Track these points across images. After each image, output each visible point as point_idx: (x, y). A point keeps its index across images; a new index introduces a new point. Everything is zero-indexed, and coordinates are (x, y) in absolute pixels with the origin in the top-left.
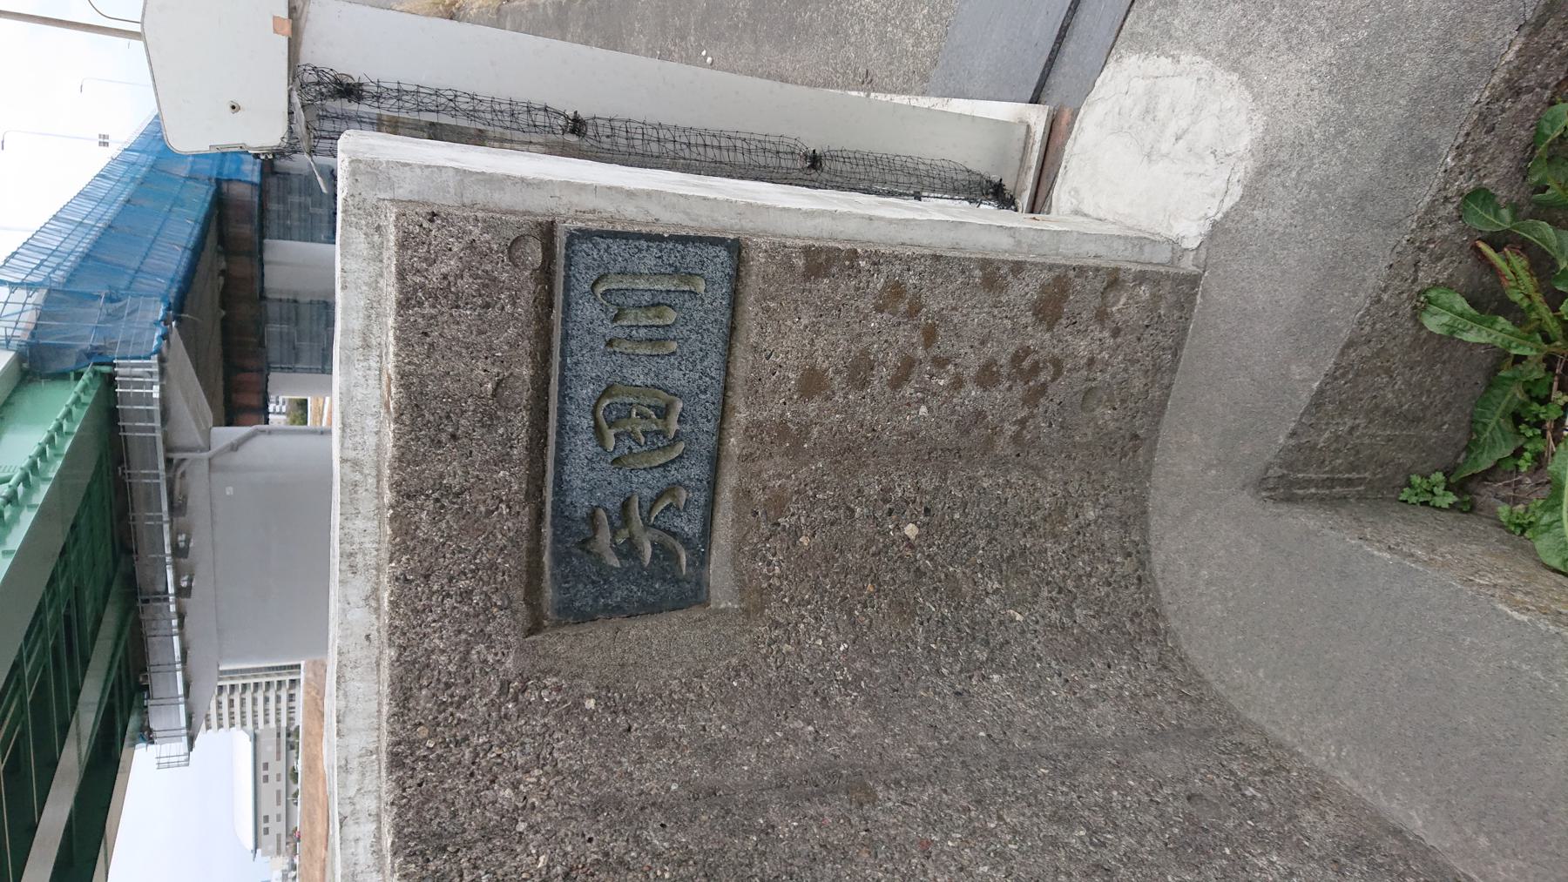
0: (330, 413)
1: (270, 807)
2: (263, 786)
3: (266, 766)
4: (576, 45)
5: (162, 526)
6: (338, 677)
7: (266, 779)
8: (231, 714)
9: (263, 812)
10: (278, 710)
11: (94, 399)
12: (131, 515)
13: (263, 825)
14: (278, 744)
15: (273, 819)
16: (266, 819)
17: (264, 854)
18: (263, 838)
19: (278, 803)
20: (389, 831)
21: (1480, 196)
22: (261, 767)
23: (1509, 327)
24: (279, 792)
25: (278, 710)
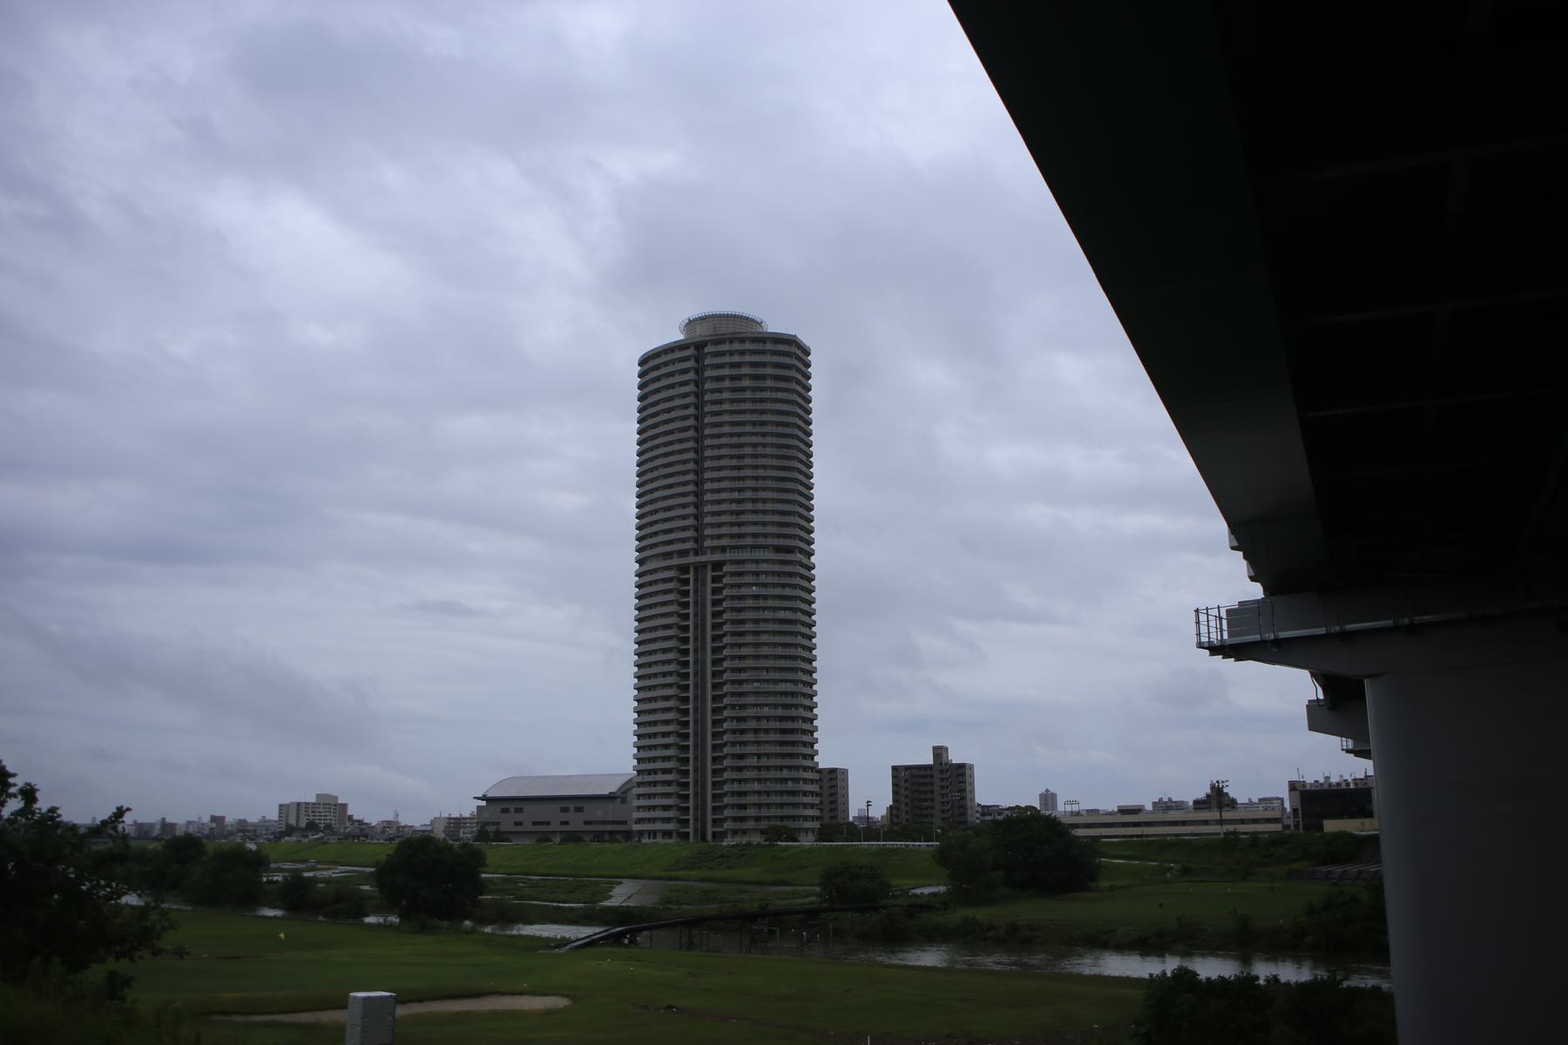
0: (702, 880)
1: (531, 814)
2: (557, 806)
5: (1228, 628)
6: (1177, 809)
8: (655, 771)
9: (527, 807)
10: (654, 820)
11: (1310, 791)
13: (512, 807)
14: (603, 823)
15: (519, 817)
16: (519, 810)
17: (479, 807)
18: (498, 807)
19: (535, 823)
20: (890, 958)
24: (548, 823)
25: (654, 820)
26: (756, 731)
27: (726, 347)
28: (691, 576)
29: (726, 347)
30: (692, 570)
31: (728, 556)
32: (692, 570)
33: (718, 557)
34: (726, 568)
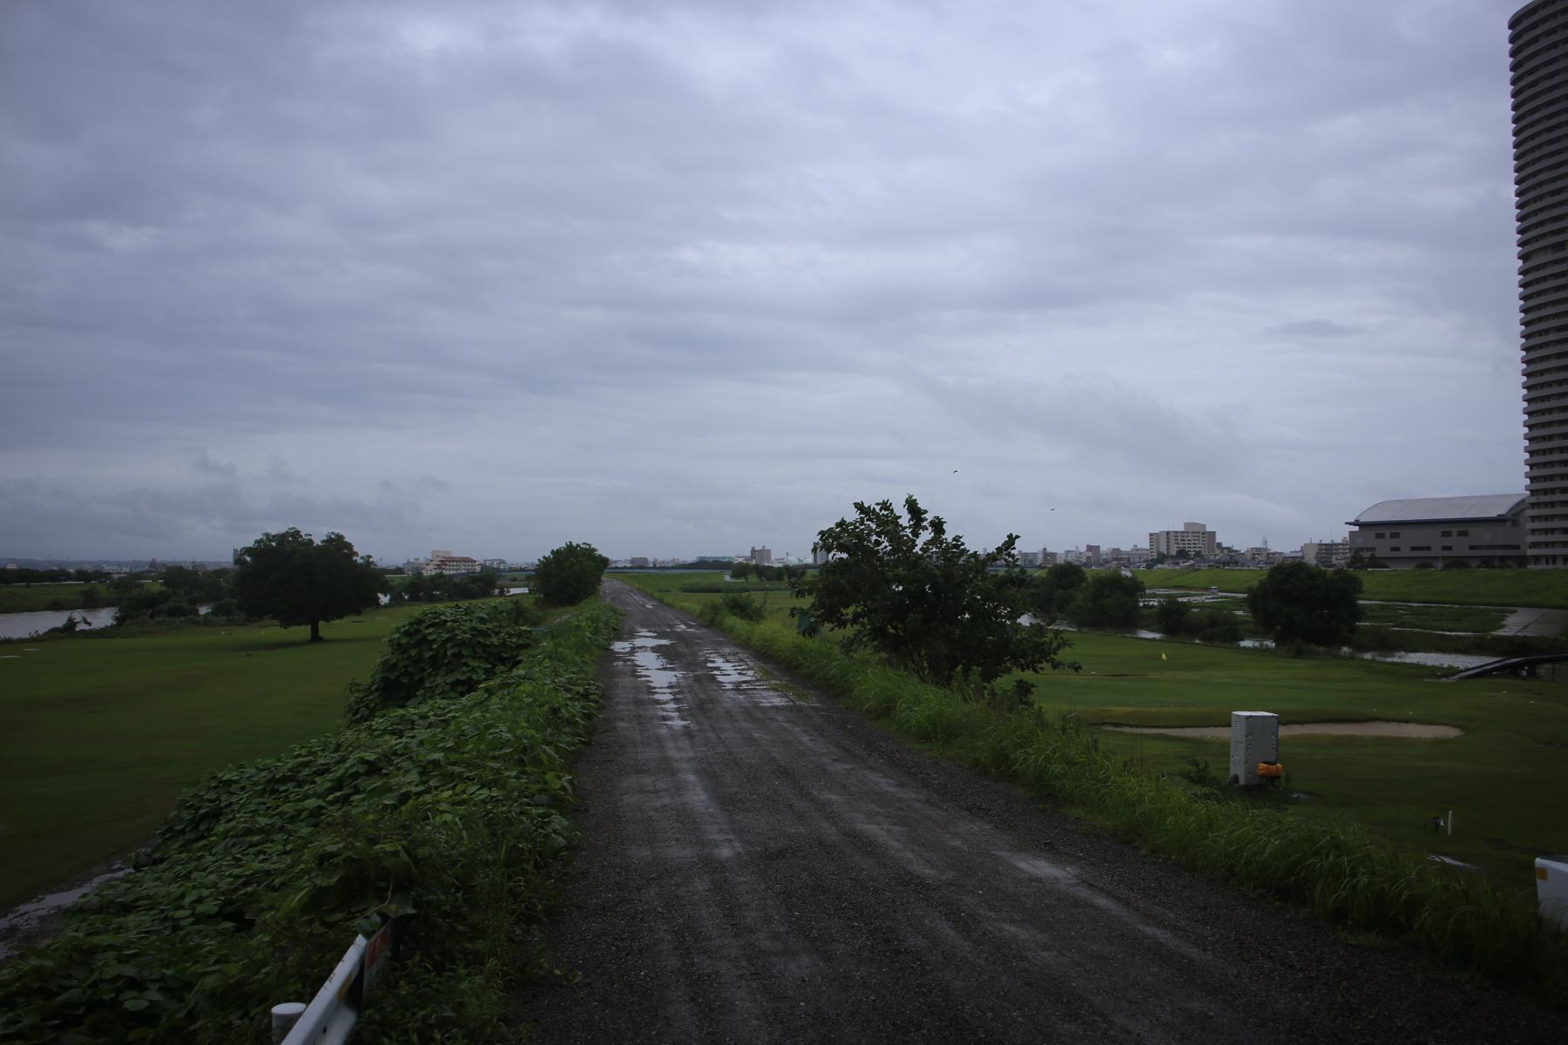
1: (1408, 539)
2: (1438, 530)
3: (1463, 534)
4: (282, 530)
7: (1446, 534)
9: (1404, 532)
10: (1553, 544)
12: (429, 571)
14: (1491, 547)
15: (1395, 542)
18: (1372, 533)
19: (1413, 549)
21: (393, 667)
22: (1463, 528)
23: (424, 571)
24: (1429, 548)
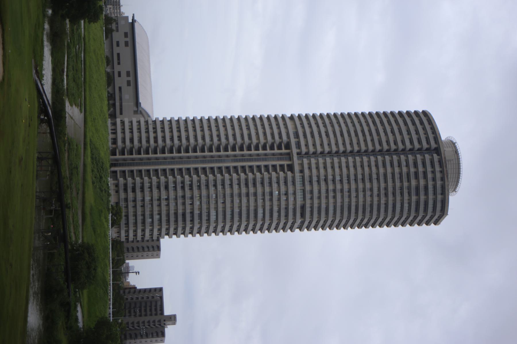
15: (122, 44)
26: (184, 197)
27: (438, 168)
28: (284, 151)
29: (438, 168)
30: (287, 151)
31: (298, 175)
32: (287, 151)
33: (297, 168)
34: (289, 173)
